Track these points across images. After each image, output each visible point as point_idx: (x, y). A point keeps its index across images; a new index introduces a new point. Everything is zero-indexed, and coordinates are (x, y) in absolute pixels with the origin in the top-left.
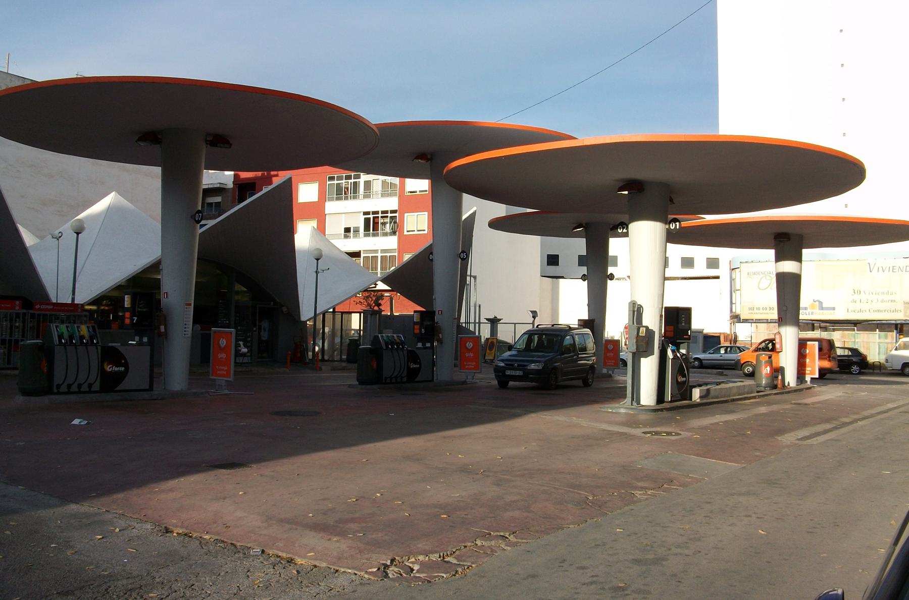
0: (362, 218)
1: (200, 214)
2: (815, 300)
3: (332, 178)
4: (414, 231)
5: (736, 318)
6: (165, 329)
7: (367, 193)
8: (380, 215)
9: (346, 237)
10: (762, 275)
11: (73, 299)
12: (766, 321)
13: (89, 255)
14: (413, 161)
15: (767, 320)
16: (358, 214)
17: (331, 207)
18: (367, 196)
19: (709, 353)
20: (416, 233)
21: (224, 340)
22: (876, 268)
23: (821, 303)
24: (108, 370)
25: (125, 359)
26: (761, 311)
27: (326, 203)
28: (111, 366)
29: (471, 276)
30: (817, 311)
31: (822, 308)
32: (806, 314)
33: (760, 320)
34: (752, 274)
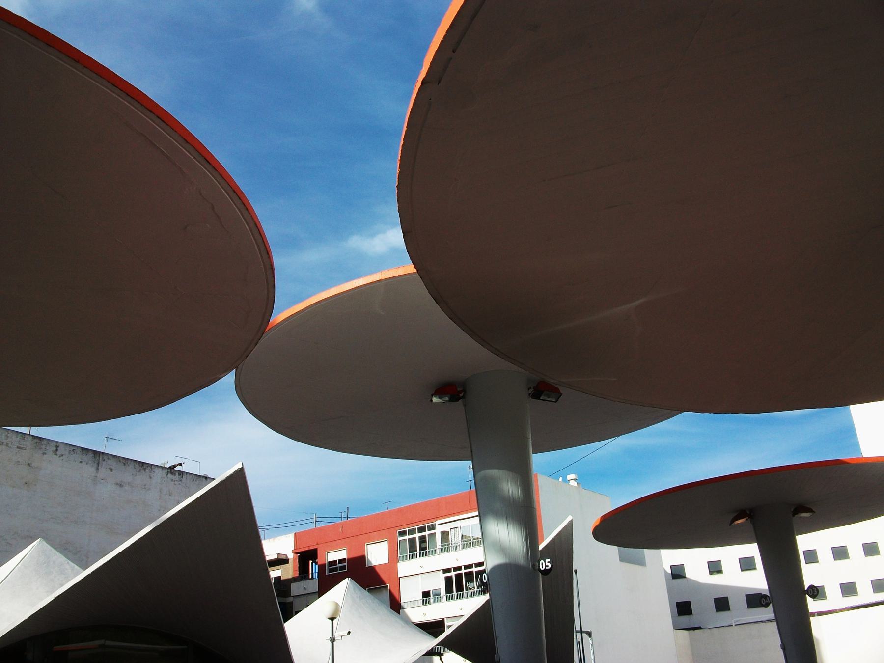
0: (442, 576)
3: (403, 534)
7: (445, 545)
8: (463, 571)
9: (426, 603)
11: (813, 614)
17: (405, 567)
18: (446, 549)
27: (398, 564)
29: (582, 632)
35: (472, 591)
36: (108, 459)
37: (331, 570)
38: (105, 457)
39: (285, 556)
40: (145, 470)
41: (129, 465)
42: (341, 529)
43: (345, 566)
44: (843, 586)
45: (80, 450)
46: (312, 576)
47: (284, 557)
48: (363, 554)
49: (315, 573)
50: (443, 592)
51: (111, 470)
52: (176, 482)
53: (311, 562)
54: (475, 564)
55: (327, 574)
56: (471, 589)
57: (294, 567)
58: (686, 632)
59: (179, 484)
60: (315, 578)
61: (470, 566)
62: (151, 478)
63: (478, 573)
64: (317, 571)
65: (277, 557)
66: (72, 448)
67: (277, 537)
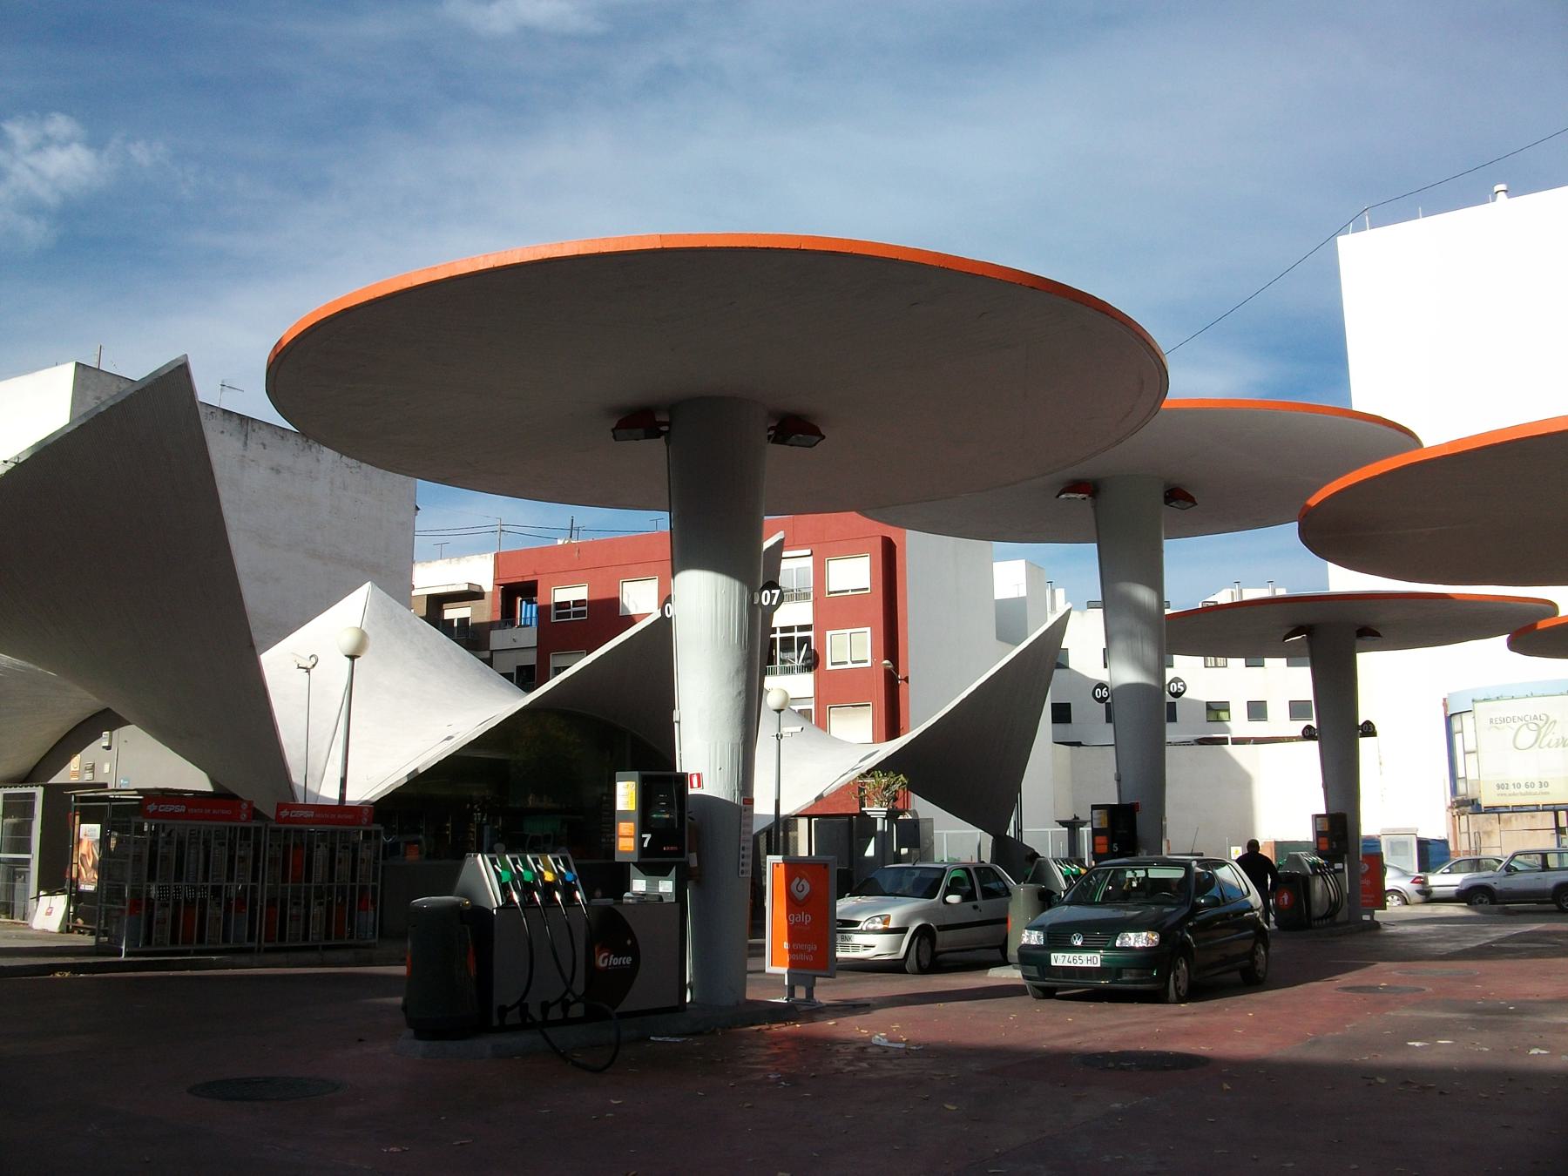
1: (777, 592)
4: (846, 663)
5: (1466, 805)
8: (778, 635)
10: (1521, 723)
11: (342, 795)
12: (1534, 808)
15: (1538, 805)
19: (1443, 873)
20: (850, 665)
21: (804, 882)
24: (602, 965)
25: (631, 935)
26: (1523, 789)
28: (606, 954)
36: (260, 428)
37: (558, 616)
38: (256, 426)
40: (310, 449)
41: (288, 440)
42: (577, 553)
43: (585, 611)
45: (220, 413)
46: (521, 623)
47: (476, 589)
48: (617, 596)
49: (531, 617)
51: (264, 446)
52: (353, 470)
53: (519, 599)
54: (798, 626)
55: (828, 668)
57: (493, 605)
58: (1068, 748)
59: (357, 472)
60: (531, 625)
61: (790, 629)
62: (318, 460)
64: (534, 615)
65: (466, 589)
66: (210, 410)
67: (464, 557)
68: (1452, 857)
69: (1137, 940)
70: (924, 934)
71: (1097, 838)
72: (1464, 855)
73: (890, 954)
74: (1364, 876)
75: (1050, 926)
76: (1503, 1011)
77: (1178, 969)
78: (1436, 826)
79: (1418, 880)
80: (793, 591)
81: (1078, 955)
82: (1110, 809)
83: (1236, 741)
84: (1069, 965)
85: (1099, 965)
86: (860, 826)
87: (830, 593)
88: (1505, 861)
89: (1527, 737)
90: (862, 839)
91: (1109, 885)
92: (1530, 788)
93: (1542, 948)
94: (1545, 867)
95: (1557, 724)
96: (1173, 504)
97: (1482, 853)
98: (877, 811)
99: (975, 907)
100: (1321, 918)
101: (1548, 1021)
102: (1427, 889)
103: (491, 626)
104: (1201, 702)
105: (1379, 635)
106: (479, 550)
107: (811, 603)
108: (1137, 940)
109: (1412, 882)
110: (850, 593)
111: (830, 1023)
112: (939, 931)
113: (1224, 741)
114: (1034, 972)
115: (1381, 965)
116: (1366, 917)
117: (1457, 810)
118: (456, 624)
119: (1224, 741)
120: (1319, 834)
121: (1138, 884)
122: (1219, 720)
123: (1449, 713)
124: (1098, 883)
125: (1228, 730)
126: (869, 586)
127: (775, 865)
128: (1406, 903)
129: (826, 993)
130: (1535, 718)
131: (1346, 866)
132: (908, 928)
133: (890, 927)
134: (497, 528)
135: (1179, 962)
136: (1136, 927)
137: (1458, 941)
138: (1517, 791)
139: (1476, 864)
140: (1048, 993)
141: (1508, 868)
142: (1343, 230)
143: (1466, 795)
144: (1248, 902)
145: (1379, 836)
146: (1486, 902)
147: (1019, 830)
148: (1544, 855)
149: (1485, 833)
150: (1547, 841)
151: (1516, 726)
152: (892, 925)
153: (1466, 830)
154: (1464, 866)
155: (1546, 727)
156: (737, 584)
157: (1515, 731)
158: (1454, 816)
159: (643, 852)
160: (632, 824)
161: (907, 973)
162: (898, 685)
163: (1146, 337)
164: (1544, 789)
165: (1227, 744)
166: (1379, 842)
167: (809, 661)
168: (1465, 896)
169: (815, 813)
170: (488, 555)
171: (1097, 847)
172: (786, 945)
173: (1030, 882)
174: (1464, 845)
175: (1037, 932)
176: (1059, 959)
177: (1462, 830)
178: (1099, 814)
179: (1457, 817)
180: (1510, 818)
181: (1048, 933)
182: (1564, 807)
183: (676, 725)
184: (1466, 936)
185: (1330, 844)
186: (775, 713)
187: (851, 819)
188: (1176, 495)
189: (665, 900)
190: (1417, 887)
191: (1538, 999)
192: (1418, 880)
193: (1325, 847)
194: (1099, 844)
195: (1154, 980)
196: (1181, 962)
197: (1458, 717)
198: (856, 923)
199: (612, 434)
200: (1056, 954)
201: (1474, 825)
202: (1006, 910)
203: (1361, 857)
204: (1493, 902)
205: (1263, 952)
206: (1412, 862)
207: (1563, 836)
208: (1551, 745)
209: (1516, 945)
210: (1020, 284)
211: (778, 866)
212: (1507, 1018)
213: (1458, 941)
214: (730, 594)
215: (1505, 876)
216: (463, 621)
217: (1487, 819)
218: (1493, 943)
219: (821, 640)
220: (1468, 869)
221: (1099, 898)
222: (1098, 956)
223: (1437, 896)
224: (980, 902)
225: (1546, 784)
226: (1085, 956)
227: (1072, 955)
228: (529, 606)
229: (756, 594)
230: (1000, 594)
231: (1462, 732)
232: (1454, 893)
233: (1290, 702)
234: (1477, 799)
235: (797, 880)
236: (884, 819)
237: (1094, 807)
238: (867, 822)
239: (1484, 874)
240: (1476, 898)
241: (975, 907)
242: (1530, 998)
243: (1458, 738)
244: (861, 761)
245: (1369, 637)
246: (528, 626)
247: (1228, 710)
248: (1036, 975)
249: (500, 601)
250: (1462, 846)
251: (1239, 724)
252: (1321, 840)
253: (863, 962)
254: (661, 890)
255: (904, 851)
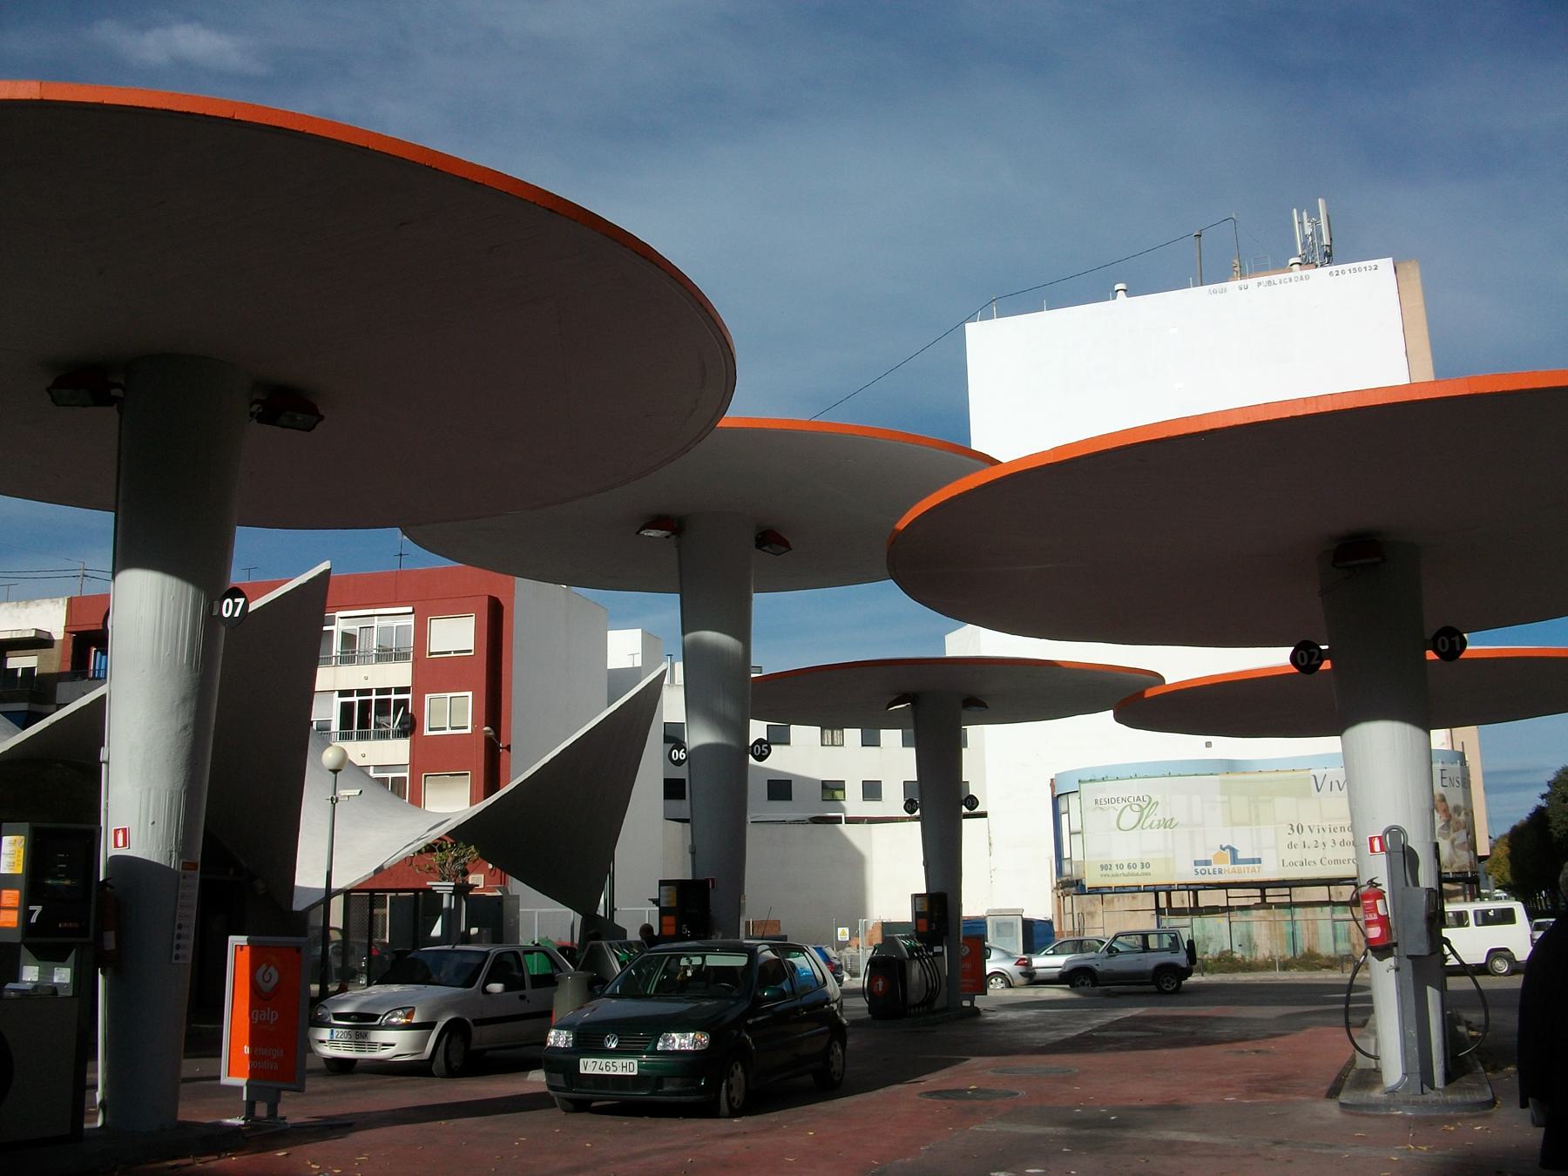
0: (337, 701)
1: (241, 601)
2: (1224, 846)
4: (444, 729)
6: (118, 942)
7: (348, 652)
8: (374, 697)
10: (1124, 804)
12: (1136, 889)
13: (1200, 257)
14: (638, 533)
15: (1140, 886)
16: (330, 694)
18: (348, 658)
19: (1046, 954)
20: (449, 731)
21: (272, 970)
22: (1326, 786)
23: (1233, 851)
26: (1126, 870)
30: (1228, 866)
31: (1235, 860)
32: (1209, 874)
33: (1123, 887)
34: (1103, 802)
35: (384, 729)
39: (47, 634)
44: (1210, 743)
47: (45, 637)
50: (335, 726)
54: (377, 689)
55: (425, 734)
56: (384, 726)
58: (679, 825)
61: (387, 691)
63: (400, 703)
68: (1056, 938)
69: (681, 1041)
70: (455, 1029)
71: (665, 918)
72: (1068, 936)
73: (412, 1055)
74: (964, 959)
75: (582, 1024)
76: (1103, 1123)
77: (732, 1075)
78: (1041, 906)
79: (1022, 962)
80: (391, 650)
81: (611, 1061)
82: (680, 886)
83: (850, 821)
84: (601, 1072)
85: (635, 1073)
86: (427, 904)
87: (431, 654)
88: (1107, 942)
89: (1130, 818)
90: (427, 918)
91: (663, 973)
92: (1132, 869)
93: (1146, 1037)
94: (1146, 948)
95: (1159, 805)
96: (766, 548)
97: (1085, 934)
98: (444, 888)
99: (522, 997)
100: (918, 1005)
101: (1154, 1137)
102: (1030, 971)
103: (60, 677)
104: (817, 780)
105: (986, 707)
106: (52, 595)
107: (411, 664)
108: (681, 1041)
109: (1016, 965)
110: (452, 655)
111: (279, 1154)
112: (475, 1025)
113: (837, 820)
114: (560, 1080)
115: (974, 1061)
116: (966, 1003)
117: (1061, 891)
118: (20, 674)
119: (837, 820)
120: (917, 915)
121: (693, 973)
122: (835, 800)
123: (1056, 794)
124: (650, 974)
125: (843, 810)
126: (472, 648)
127: (239, 948)
128: (1009, 985)
129: (294, 1110)
130: (1138, 799)
131: (945, 948)
132: (436, 1023)
133: (413, 1021)
134: (80, 573)
135: (734, 1067)
136: (683, 1028)
137: (1058, 1029)
138: (1120, 871)
139: (1079, 946)
140: (580, 1106)
141: (1110, 949)
142: (972, 318)
143: (1071, 875)
144: (826, 993)
145: (985, 917)
146: (1088, 985)
147: (612, 909)
148: (1145, 936)
149: (1088, 914)
150: (1147, 922)
151: (1120, 806)
152: (416, 1019)
153: (1071, 911)
154: (1068, 947)
155: (1148, 809)
156: (191, 589)
157: (1118, 812)
158: (1059, 897)
159: (26, 926)
160: (17, 892)
161: (433, 1076)
162: (500, 754)
163: (727, 338)
164: (1145, 870)
165: (841, 823)
166: (985, 923)
167: (406, 726)
168: (1068, 977)
169: (377, 887)
170: (61, 601)
171: (664, 929)
172: (247, 1050)
173: (581, 970)
174: (1068, 927)
175: (565, 1032)
176: (590, 1066)
177: (1067, 911)
178: (667, 890)
179: (1062, 898)
180: (1113, 898)
181: (578, 1034)
182: (1163, 888)
183: (104, 765)
184: (1069, 1023)
185: (929, 927)
186: (331, 773)
187: (416, 894)
188: (770, 539)
189: (61, 994)
190: (1020, 969)
191: (1141, 1104)
192: (1022, 962)
193: (924, 929)
194: (666, 925)
195: (701, 1090)
196: (737, 1068)
197: (1064, 797)
198: (375, 1017)
199: (49, 398)
200: (586, 1060)
201: (1078, 905)
202: (550, 1001)
203: (961, 939)
204: (1095, 984)
205: (839, 1051)
206: (1017, 944)
207: (1163, 917)
208: (1153, 826)
209: (1118, 1034)
210: (535, 203)
211: (242, 949)
212: (1108, 1133)
213: (1058, 1029)
214: (181, 602)
215: (1106, 958)
216: (28, 671)
217: (1091, 901)
218: (1094, 1031)
219: (419, 703)
220: (1072, 951)
221: (651, 990)
222: (635, 1062)
223: (1041, 978)
224: (528, 991)
225: (1148, 865)
226: (619, 1062)
227: (605, 1061)
228: (104, 657)
229: (216, 603)
230: (613, 664)
231: (1068, 812)
232: (1057, 975)
233: (904, 782)
234: (1081, 880)
235: (264, 967)
236: (451, 895)
237: (662, 883)
238: (434, 898)
239: (1087, 955)
240: (1079, 980)
241: (522, 997)
242: (1134, 1103)
243: (1064, 818)
244: (429, 830)
245: (975, 708)
246: (101, 679)
247: (843, 789)
248: (562, 1085)
249: (71, 650)
250: (1065, 927)
251: (854, 803)
252: (920, 921)
253: (382, 1063)
254: (56, 980)
255: (474, 931)
